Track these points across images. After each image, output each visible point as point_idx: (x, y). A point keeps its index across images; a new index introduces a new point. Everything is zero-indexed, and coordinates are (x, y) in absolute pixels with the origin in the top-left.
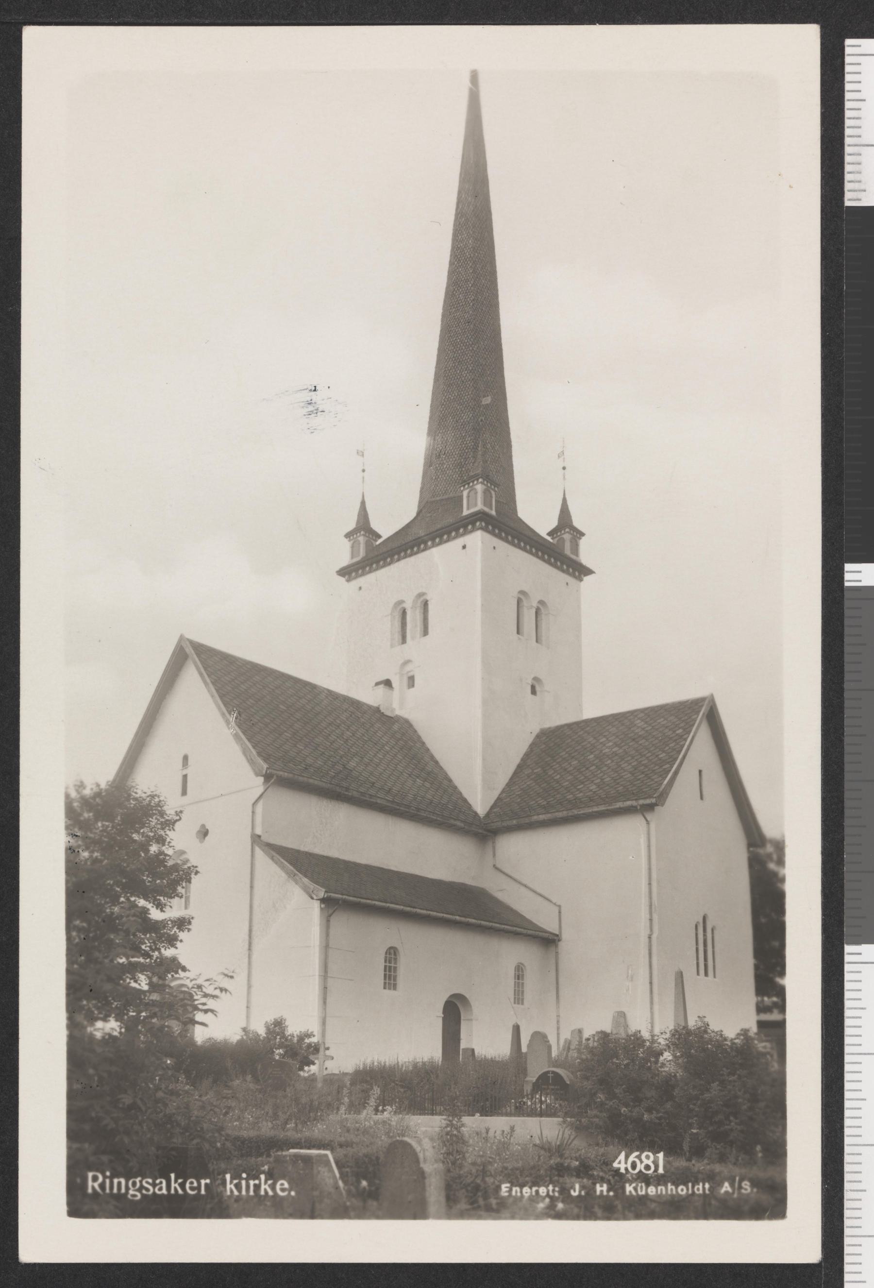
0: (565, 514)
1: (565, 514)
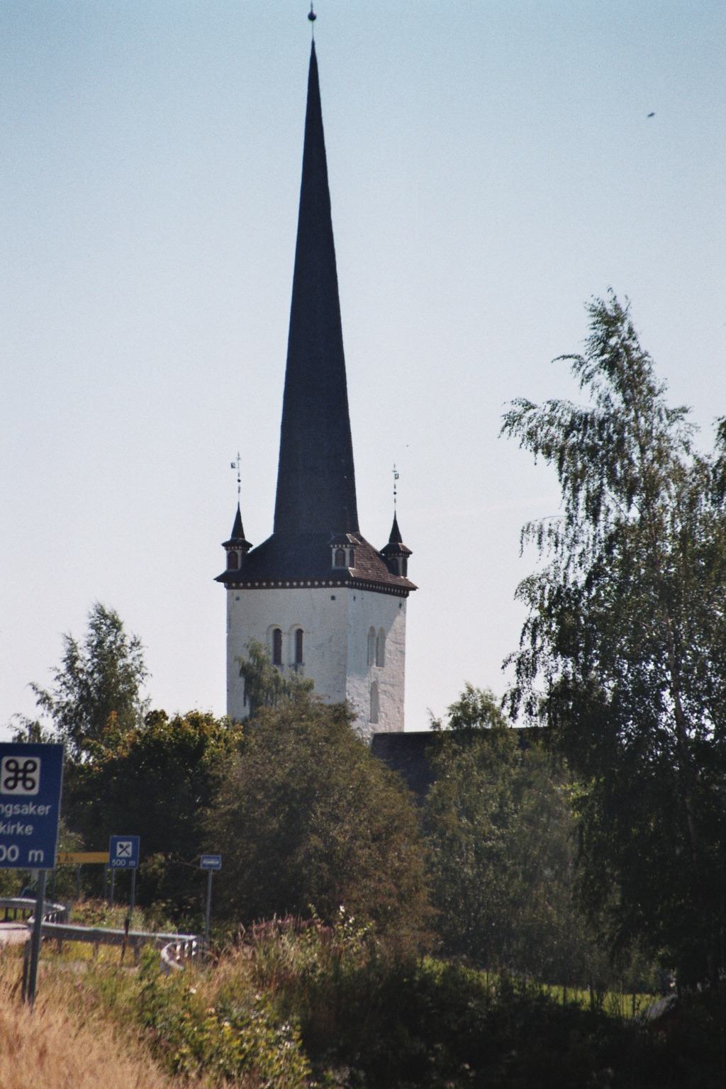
0: (395, 535)
1: (395, 535)
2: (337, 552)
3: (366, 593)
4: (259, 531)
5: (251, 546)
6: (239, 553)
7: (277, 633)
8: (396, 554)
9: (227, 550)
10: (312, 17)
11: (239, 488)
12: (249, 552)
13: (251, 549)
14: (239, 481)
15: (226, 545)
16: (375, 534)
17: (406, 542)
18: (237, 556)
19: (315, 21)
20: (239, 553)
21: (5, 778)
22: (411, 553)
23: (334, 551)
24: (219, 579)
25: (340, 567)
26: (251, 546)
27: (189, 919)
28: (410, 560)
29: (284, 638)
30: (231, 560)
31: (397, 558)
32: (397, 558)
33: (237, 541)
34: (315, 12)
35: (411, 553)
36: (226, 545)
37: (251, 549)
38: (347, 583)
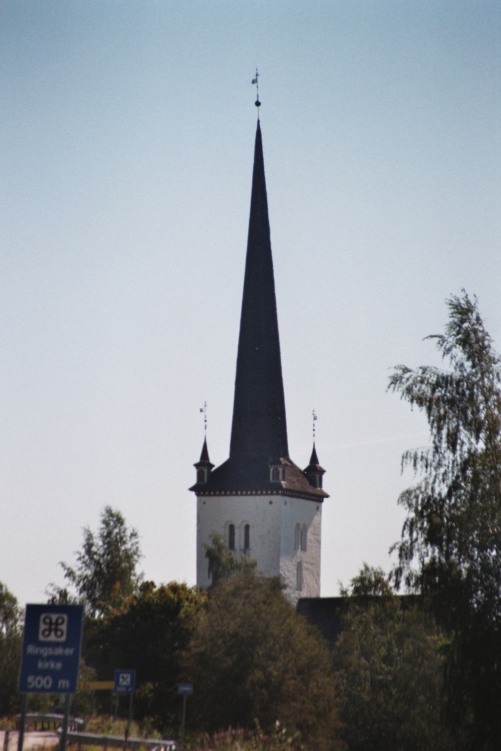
0: (314, 459)
1: (314, 459)
4: (220, 456)
5: (213, 466)
6: (205, 471)
7: (232, 528)
8: (314, 472)
10: (258, 104)
11: (206, 426)
13: (214, 469)
14: (206, 421)
15: (196, 465)
16: (300, 458)
19: (260, 107)
20: (205, 471)
22: (325, 472)
23: (271, 470)
24: (192, 489)
25: (276, 481)
28: (324, 477)
29: (237, 531)
30: (200, 476)
33: (204, 463)
34: (260, 101)
35: (325, 472)
36: (196, 465)
37: (214, 469)
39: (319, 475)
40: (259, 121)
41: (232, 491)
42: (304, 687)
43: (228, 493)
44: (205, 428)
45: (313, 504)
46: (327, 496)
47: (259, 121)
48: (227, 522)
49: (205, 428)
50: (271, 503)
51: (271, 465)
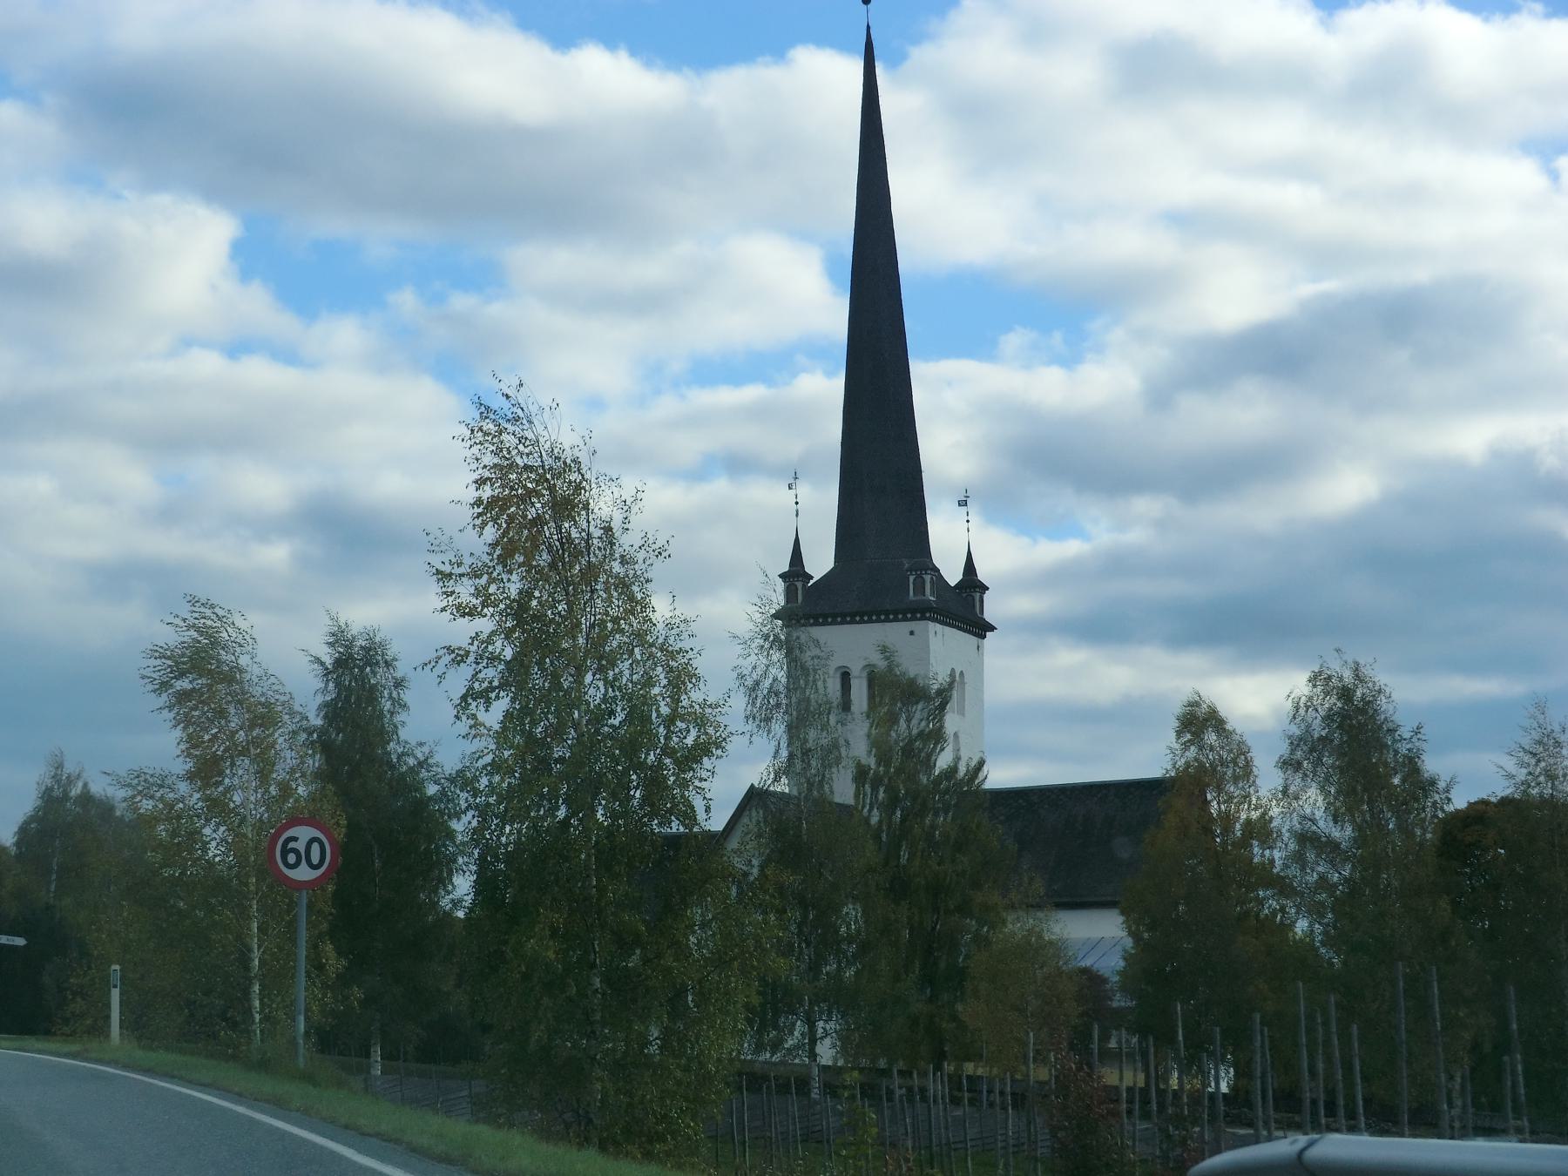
0: (970, 567)
1: (970, 567)
2: (915, 580)
3: (947, 629)
4: (820, 562)
5: (812, 578)
6: (799, 585)
7: (845, 677)
8: (972, 584)
9: (784, 582)
11: (797, 511)
12: (809, 585)
13: (812, 582)
15: (783, 576)
17: (982, 575)
18: (797, 589)
20: (799, 585)
21: (289, 836)
22: (988, 589)
23: (912, 579)
25: (920, 597)
26: (812, 578)
27: (218, 825)
29: (855, 683)
30: (790, 593)
31: (973, 594)
32: (973, 594)
33: (795, 572)
35: (988, 589)
36: (783, 576)
37: (812, 582)
38: (928, 615)
39: (978, 594)
40: (868, 27)
41: (897, 614)
42: (1185, 1132)
43: (874, 618)
44: (797, 515)
45: (973, 640)
46: (992, 628)
47: (868, 27)
48: (848, 668)
49: (797, 515)
50: (912, 633)
51: (911, 571)
